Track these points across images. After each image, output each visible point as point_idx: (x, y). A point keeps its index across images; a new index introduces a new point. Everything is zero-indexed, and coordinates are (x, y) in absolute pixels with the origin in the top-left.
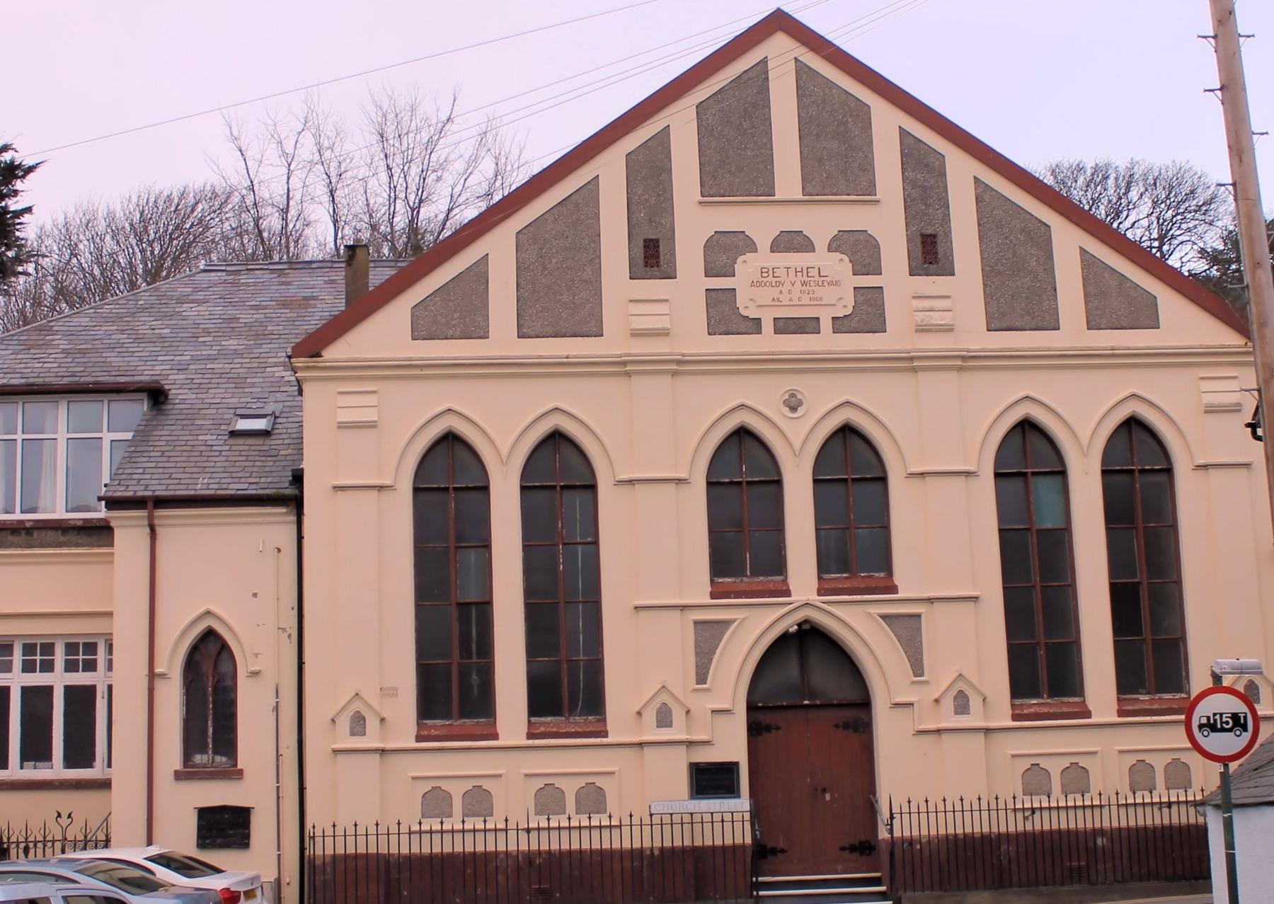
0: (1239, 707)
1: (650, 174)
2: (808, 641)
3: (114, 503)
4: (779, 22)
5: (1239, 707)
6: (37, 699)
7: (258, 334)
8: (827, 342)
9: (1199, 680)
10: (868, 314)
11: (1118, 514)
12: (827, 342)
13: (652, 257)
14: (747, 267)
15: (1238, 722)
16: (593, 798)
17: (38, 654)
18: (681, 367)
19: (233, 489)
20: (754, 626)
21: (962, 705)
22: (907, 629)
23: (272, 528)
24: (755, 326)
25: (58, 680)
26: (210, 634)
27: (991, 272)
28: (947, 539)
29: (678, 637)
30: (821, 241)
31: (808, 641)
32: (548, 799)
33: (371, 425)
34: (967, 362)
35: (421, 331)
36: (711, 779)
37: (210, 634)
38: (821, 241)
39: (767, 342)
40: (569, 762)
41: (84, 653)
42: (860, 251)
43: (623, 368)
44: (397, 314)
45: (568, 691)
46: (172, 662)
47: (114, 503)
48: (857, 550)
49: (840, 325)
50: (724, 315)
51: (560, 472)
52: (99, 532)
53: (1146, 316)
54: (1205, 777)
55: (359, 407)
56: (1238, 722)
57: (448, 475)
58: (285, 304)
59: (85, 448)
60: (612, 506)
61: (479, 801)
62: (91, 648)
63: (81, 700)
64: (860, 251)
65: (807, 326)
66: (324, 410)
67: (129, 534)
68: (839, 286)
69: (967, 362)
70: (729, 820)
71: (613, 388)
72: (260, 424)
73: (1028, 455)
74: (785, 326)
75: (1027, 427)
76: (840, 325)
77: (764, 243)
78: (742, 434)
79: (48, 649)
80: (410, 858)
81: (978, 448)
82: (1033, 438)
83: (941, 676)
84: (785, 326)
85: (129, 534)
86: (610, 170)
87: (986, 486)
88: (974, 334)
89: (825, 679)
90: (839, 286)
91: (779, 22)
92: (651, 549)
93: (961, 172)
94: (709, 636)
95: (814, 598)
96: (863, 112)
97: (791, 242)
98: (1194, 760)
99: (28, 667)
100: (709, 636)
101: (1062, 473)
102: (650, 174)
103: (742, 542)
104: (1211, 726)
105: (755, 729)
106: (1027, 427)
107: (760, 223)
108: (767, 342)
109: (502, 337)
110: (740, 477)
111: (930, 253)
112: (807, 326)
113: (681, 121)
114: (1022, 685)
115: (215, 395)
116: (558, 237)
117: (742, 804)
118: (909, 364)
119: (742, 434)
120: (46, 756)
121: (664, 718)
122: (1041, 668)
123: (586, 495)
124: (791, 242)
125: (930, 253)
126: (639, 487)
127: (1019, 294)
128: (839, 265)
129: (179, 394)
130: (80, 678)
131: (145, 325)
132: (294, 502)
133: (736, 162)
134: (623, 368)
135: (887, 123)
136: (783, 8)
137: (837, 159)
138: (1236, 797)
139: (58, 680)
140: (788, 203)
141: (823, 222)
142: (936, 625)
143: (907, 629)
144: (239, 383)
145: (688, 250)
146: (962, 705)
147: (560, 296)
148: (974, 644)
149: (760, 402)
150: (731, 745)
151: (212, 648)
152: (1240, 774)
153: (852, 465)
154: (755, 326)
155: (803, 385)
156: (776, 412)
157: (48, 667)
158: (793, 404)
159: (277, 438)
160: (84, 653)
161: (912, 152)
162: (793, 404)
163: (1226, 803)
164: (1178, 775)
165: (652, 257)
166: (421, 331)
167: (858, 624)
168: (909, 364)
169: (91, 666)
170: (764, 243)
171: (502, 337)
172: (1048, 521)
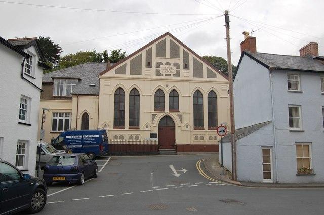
0: (224, 129)
1: (149, 53)
2: (167, 118)
3: (72, 94)
4: (168, 34)
5: (224, 129)
6: (61, 121)
7: (94, 73)
8: (172, 78)
9: (219, 125)
10: (178, 74)
11: (209, 103)
12: (172, 78)
13: (149, 65)
14: (162, 67)
15: (224, 131)
16: (137, 137)
17: (61, 115)
18: (152, 80)
19: (91, 93)
20: (160, 115)
21: (187, 127)
22: (180, 117)
23: (95, 99)
24: (162, 75)
25: (64, 118)
26: (85, 113)
27: (195, 69)
28: (186, 105)
29: (150, 116)
30: (172, 64)
31: (167, 118)
32: (131, 137)
33: (109, 85)
34: (190, 81)
35: (117, 72)
36: (153, 135)
37: (85, 113)
38: (172, 64)
39: (164, 77)
40: (134, 132)
41: (68, 115)
42: (177, 66)
43: (144, 80)
44: (114, 70)
45: (135, 124)
46: (80, 117)
47: (72, 94)
48: (174, 106)
49: (174, 75)
50: (158, 73)
51: (135, 93)
52: (71, 98)
53: (215, 76)
54: (219, 138)
55: (108, 83)
56: (224, 131)
57: (119, 93)
58: (99, 68)
59: (69, 87)
60: (142, 98)
61: (122, 137)
62: (69, 114)
63: (67, 121)
64: (177, 66)
65: (169, 75)
66: (103, 83)
67: (75, 99)
68: (174, 70)
69: (190, 81)
70: (155, 141)
71: (142, 82)
72: (94, 85)
73: (198, 94)
74: (166, 75)
75: (198, 91)
76: (174, 75)
77: (164, 64)
78: (160, 89)
79: (63, 114)
80: (154, 145)
81: (112, 90)
82: (199, 93)
83: (185, 123)
84: (166, 75)
85: (75, 99)
86: (144, 52)
87: (113, 96)
88: (192, 78)
89: (170, 124)
90: (174, 70)
91: (168, 34)
92: (147, 104)
93: (191, 56)
94: (154, 116)
95: (168, 112)
96: (178, 47)
97: (168, 64)
98: (218, 136)
99: (60, 116)
100: (154, 116)
101: (202, 97)
102: (149, 53)
103: (159, 106)
104: (220, 131)
105: (159, 129)
106: (198, 91)
107: (164, 61)
108: (164, 77)
109: (128, 75)
110: (159, 94)
111: (186, 66)
112: (169, 75)
113: (154, 46)
114: (195, 125)
115: (88, 80)
116: (138, 61)
117: (157, 139)
118: (183, 81)
119: (160, 89)
120: (62, 129)
121: (147, 127)
122: (198, 123)
123: (138, 97)
124: (168, 64)
125: (186, 66)
126: (145, 96)
127: (198, 73)
128: (174, 67)
129: (82, 79)
130: (67, 118)
131: (79, 70)
132: (98, 95)
133: (161, 52)
134: (144, 80)
135: (181, 48)
136: (257, 41)
137: (175, 53)
138: (223, 141)
139: (64, 118)
140: (168, 58)
141: (172, 61)
142: (185, 117)
143: (180, 117)
144: (91, 79)
145: (154, 64)
146: (187, 127)
147: (136, 69)
148: (189, 119)
149: (162, 85)
150: (156, 131)
151: (86, 115)
152: (225, 138)
153: (174, 94)
154: (162, 75)
155: (168, 83)
156: (165, 87)
157: (63, 116)
158: (167, 86)
159: (96, 87)
160: (68, 115)
161: (185, 53)
162: (167, 86)
163: (222, 142)
164: (215, 138)
165: (149, 65)
166: (117, 72)
167: (174, 116)
168: (183, 81)
169: (69, 117)
170: (164, 64)
171: (128, 75)
172: (200, 103)
